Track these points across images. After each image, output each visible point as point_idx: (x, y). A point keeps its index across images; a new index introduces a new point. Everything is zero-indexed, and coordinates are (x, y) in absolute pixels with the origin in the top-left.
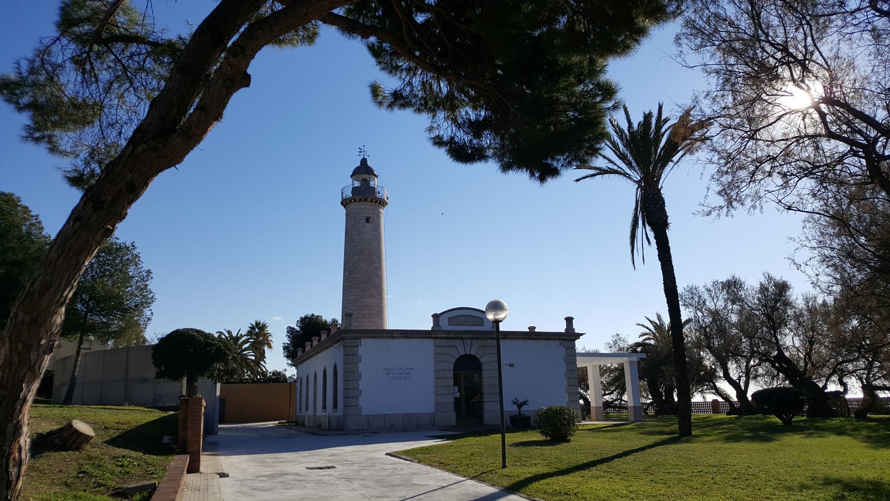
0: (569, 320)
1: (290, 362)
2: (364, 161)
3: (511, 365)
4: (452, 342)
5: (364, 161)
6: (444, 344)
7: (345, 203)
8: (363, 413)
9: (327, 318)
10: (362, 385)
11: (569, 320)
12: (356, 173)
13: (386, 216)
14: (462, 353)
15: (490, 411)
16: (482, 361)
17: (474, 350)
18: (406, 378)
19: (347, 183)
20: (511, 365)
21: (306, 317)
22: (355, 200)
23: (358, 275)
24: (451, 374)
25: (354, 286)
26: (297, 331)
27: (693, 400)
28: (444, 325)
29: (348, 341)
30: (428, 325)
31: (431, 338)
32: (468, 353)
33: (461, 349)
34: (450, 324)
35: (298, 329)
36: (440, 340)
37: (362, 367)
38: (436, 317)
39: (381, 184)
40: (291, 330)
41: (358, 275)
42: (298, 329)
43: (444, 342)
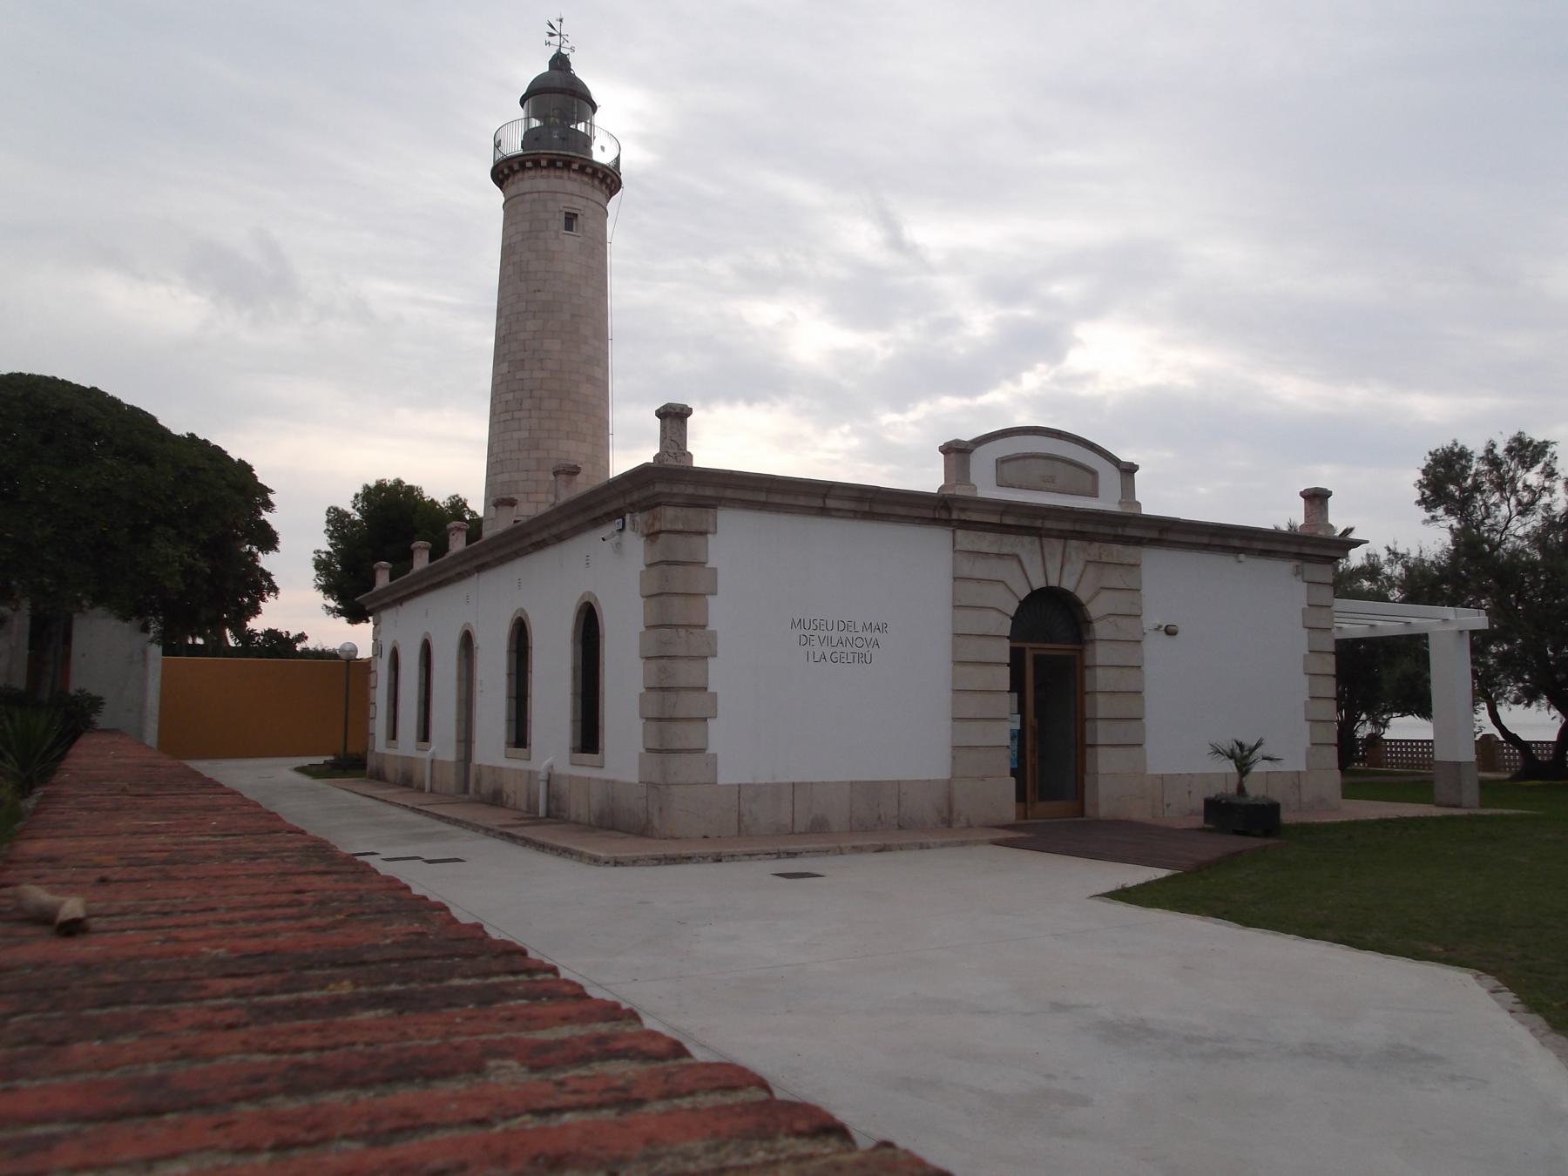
0: (1316, 499)
1: (332, 603)
2: (560, 62)
3: (1170, 632)
4: (1010, 543)
5: (560, 62)
6: (984, 547)
7: (503, 172)
8: (726, 777)
9: (437, 491)
10: (719, 675)
11: (1316, 499)
12: (535, 95)
13: (623, 224)
14: (1038, 583)
15: (1112, 779)
16: (1094, 610)
17: (1070, 571)
18: (862, 658)
19: (509, 125)
20: (1170, 632)
21: (380, 486)
22: (537, 164)
23: (538, 374)
24: (1002, 651)
25: (527, 403)
26: (354, 523)
27: (1359, 736)
28: (986, 487)
29: (670, 512)
30: (929, 478)
31: (946, 523)
32: (1053, 582)
33: (1039, 567)
34: (1002, 483)
35: (357, 517)
36: (972, 535)
37: (720, 613)
38: (957, 452)
39: (613, 132)
40: (337, 518)
41: (538, 374)
42: (357, 517)
43: (987, 542)
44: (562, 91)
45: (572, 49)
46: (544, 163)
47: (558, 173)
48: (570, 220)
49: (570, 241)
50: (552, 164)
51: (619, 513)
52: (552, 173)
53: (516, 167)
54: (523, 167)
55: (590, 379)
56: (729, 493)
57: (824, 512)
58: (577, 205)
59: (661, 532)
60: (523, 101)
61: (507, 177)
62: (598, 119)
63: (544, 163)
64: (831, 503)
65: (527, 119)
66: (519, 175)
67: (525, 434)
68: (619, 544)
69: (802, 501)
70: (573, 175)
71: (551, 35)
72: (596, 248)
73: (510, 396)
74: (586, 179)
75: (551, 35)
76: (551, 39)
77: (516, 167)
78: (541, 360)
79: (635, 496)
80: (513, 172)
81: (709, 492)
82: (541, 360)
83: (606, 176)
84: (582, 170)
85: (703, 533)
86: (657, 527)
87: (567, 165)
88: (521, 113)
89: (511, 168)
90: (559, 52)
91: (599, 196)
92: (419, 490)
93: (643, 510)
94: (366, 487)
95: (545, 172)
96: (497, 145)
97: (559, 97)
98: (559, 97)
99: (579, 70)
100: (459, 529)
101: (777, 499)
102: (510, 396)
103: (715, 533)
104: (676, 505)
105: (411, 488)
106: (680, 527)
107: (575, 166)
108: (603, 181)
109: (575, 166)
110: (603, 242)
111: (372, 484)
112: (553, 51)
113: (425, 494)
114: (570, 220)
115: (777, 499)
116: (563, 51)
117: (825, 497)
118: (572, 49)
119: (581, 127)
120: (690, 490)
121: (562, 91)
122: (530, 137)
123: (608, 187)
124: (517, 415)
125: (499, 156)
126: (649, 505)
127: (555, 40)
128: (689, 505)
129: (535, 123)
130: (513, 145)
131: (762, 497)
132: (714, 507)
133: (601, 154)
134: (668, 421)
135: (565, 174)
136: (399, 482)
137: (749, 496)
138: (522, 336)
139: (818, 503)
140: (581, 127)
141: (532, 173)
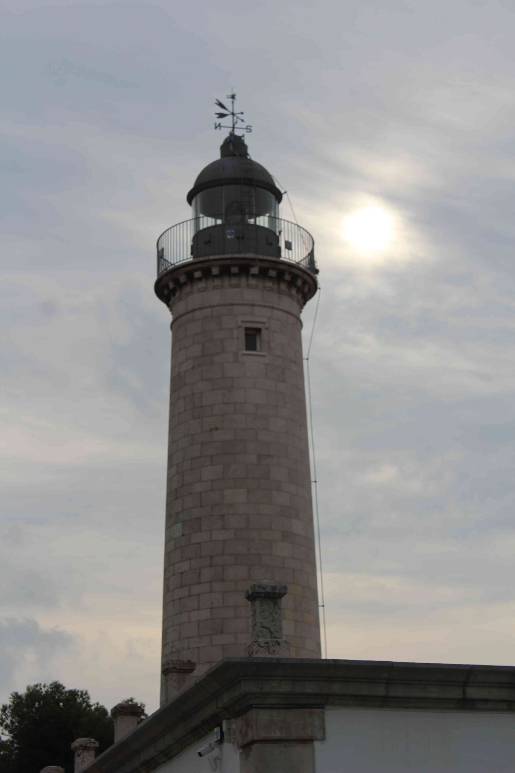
2: (234, 147)
5: (234, 147)
7: (170, 285)
9: (105, 696)
12: (206, 190)
19: (174, 226)
21: (34, 694)
22: (207, 274)
29: (263, 716)
44: (235, 181)
45: (249, 129)
46: (215, 271)
47: (234, 281)
48: (252, 336)
49: (253, 363)
50: (225, 271)
51: (214, 721)
52: (226, 281)
53: (183, 279)
54: (191, 279)
55: (287, 536)
56: (336, 688)
57: (466, 704)
58: (260, 317)
59: (254, 742)
60: (190, 197)
61: (173, 292)
62: (284, 210)
63: (215, 271)
64: (473, 693)
65: (197, 219)
66: (187, 289)
67: (205, 614)
68: (217, 760)
69: (434, 692)
70: (253, 282)
71: (222, 116)
72: (289, 367)
73: (185, 566)
74: (269, 284)
75: (222, 116)
76: (223, 121)
77: (183, 279)
78: (222, 517)
79: (225, 699)
80: (180, 285)
81: (311, 688)
82: (222, 517)
83: (295, 277)
84: (263, 274)
85: (308, 741)
86: (249, 738)
87: (244, 269)
88: (188, 212)
89: (176, 281)
90: (232, 135)
91: (288, 303)
92: (84, 695)
93: (237, 714)
94: (16, 697)
95: (217, 282)
96: (160, 255)
97: (236, 186)
98: (236, 186)
99: (255, 154)
100: (85, 748)
101: (399, 691)
102: (185, 566)
103: (323, 739)
104: (271, 707)
105: (73, 694)
106: (277, 734)
107: (255, 270)
108: (291, 284)
109: (255, 270)
110: (297, 360)
111: (22, 691)
112: (224, 134)
113: (92, 701)
114: (252, 336)
115: (399, 691)
116: (238, 133)
117: (464, 685)
118: (249, 129)
119: (263, 221)
120: (285, 687)
121: (235, 181)
122: (202, 240)
123: (299, 290)
124: (195, 589)
125: (163, 268)
126: (240, 709)
127: (227, 121)
128: (288, 707)
129: (207, 222)
130: (181, 253)
131: (380, 691)
132: (321, 706)
133: (294, 256)
134: (257, 603)
135: (243, 281)
136: (57, 687)
137: (364, 690)
138: (198, 488)
139: (456, 693)
140: (263, 221)
141: (202, 285)
